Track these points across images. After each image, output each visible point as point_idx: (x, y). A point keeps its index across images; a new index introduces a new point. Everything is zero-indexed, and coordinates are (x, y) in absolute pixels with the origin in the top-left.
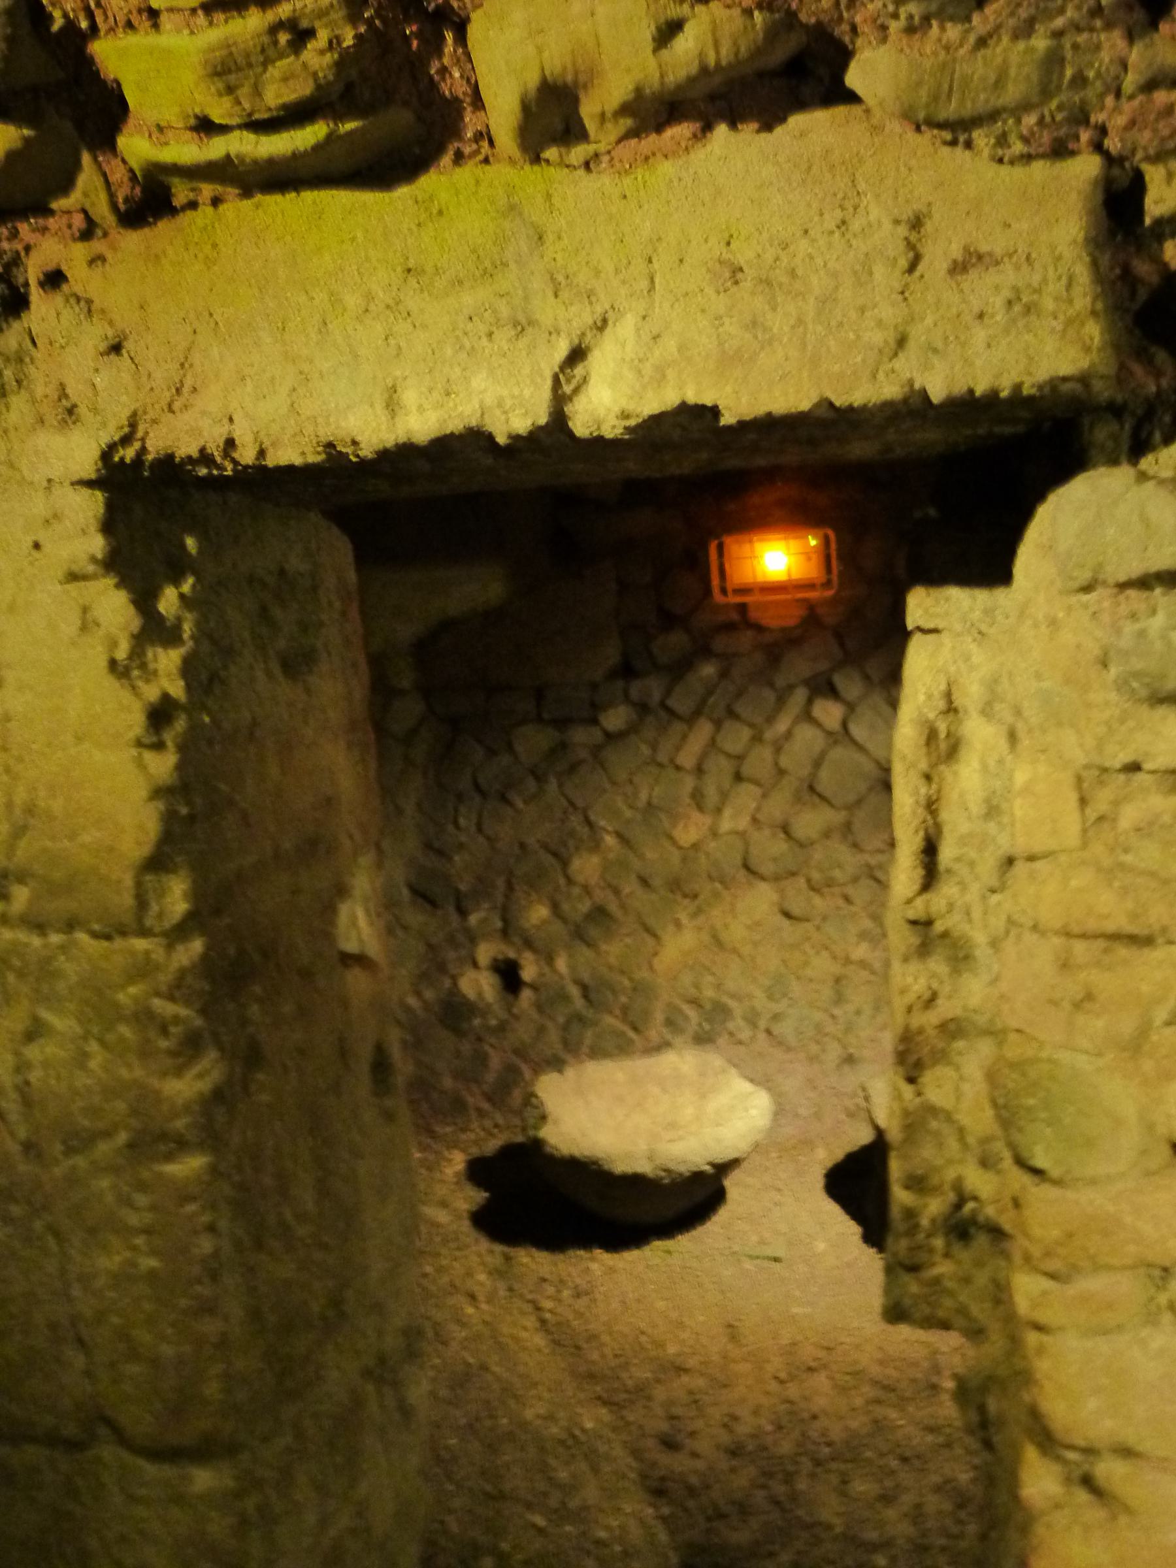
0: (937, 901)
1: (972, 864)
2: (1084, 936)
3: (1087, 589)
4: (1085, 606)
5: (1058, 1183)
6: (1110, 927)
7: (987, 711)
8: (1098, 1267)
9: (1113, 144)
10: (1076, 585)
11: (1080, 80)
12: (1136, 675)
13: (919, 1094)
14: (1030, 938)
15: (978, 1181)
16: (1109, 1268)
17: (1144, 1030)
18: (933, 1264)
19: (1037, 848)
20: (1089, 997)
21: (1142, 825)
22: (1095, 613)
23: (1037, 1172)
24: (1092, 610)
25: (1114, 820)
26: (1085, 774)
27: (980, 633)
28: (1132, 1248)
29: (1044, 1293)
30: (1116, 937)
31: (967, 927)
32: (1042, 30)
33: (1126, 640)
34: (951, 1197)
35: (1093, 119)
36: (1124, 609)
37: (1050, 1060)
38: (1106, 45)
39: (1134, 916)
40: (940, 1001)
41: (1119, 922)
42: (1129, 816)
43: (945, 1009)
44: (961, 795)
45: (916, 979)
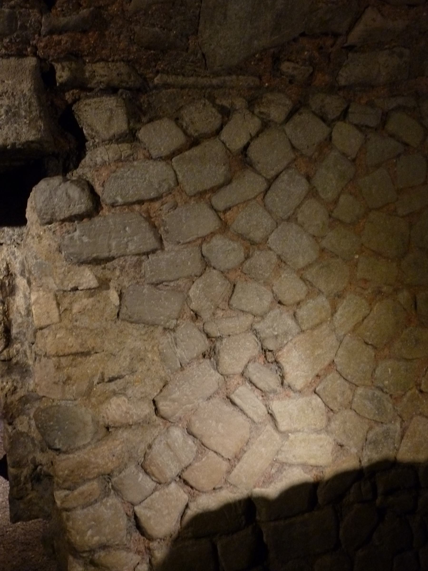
0: (13, 351)
1: (25, 334)
2: (64, 356)
3: (50, 223)
4: (50, 229)
5: (66, 452)
6: (74, 350)
7: (22, 274)
8: (85, 481)
9: (40, 53)
10: (45, 221)
11: (24, 27)
12: (71, 254)
13: (14, 428)
14: (44, 360)
15: (40, 457)
16: (89, 480)
17: (90, 388)
18: (28, 495)
19: (43, 324)
20: (69, 378)
21: (81, 310)
22: (54, 232)
23: (58, 450)
24: (53, 230)
25: (71, 310)
26: (57, 293)
27: (17, 243)
28: (96, 470)
29: (66, 496)
30: (76, 354)
31: (25, 359)
32: (6, 5)
33: (66, 242)
34: (32, 466)
35: (31, 43)
36: (64, 230)
37: (57, 406)
38: (32, 14)
39: (82, 345)
40: (18, 390)
41: (77, 348)
42: (76, 308)
43: (21, 393)
44: (17, 308)
45: (7, 383)
